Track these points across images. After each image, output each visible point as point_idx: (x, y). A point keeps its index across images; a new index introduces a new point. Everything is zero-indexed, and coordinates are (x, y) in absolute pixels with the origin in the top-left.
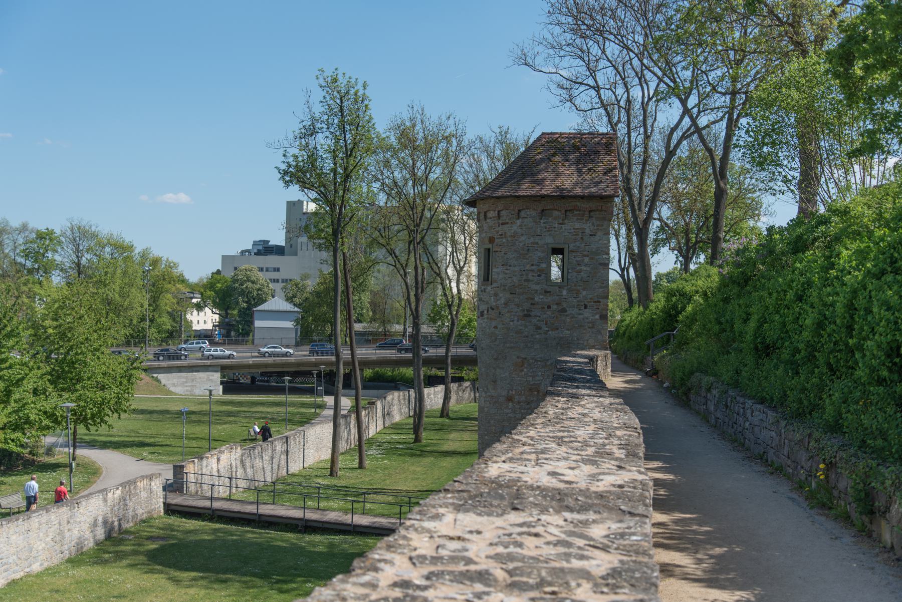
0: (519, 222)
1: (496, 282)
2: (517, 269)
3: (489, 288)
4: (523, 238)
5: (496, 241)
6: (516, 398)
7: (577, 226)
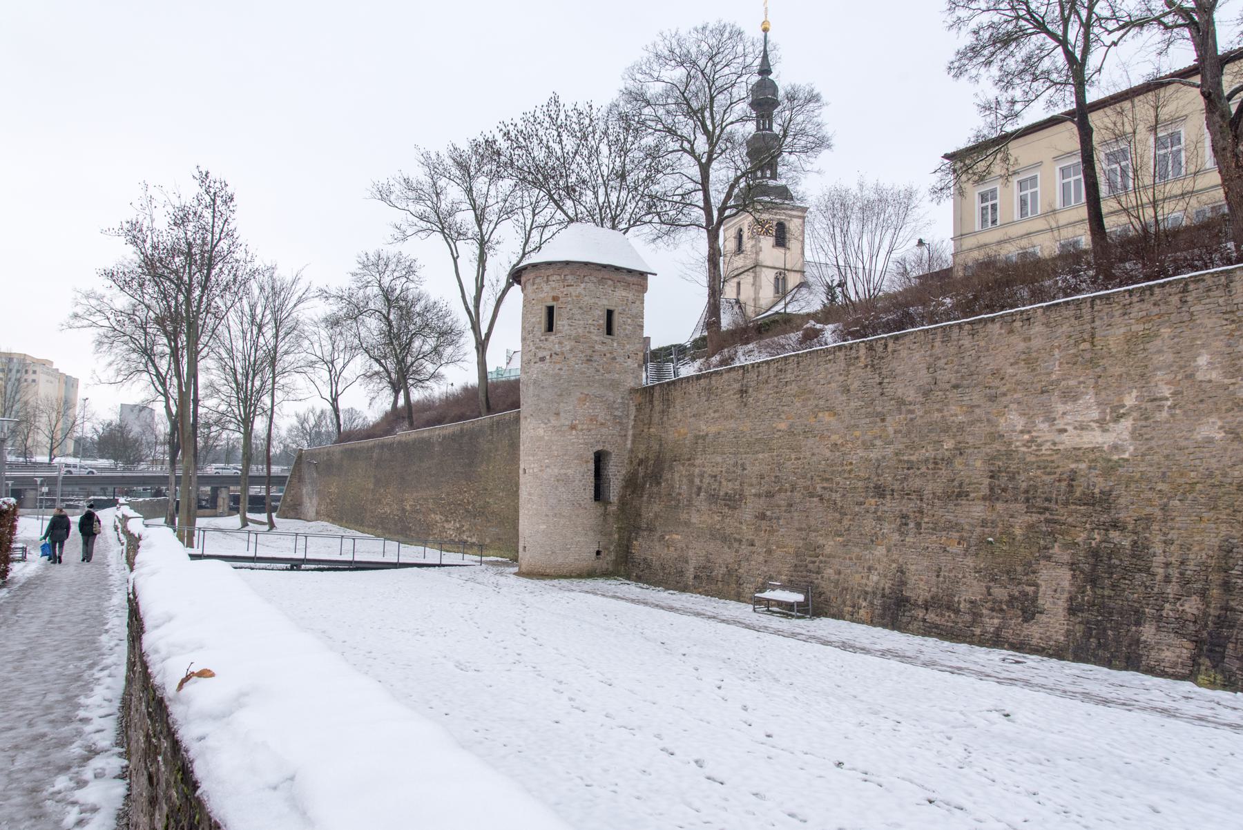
0: (583, 286)
2: (581, 322)
3: (553, 337)
4: (586, 298)
6: (580, 427)
7: (624, 294)
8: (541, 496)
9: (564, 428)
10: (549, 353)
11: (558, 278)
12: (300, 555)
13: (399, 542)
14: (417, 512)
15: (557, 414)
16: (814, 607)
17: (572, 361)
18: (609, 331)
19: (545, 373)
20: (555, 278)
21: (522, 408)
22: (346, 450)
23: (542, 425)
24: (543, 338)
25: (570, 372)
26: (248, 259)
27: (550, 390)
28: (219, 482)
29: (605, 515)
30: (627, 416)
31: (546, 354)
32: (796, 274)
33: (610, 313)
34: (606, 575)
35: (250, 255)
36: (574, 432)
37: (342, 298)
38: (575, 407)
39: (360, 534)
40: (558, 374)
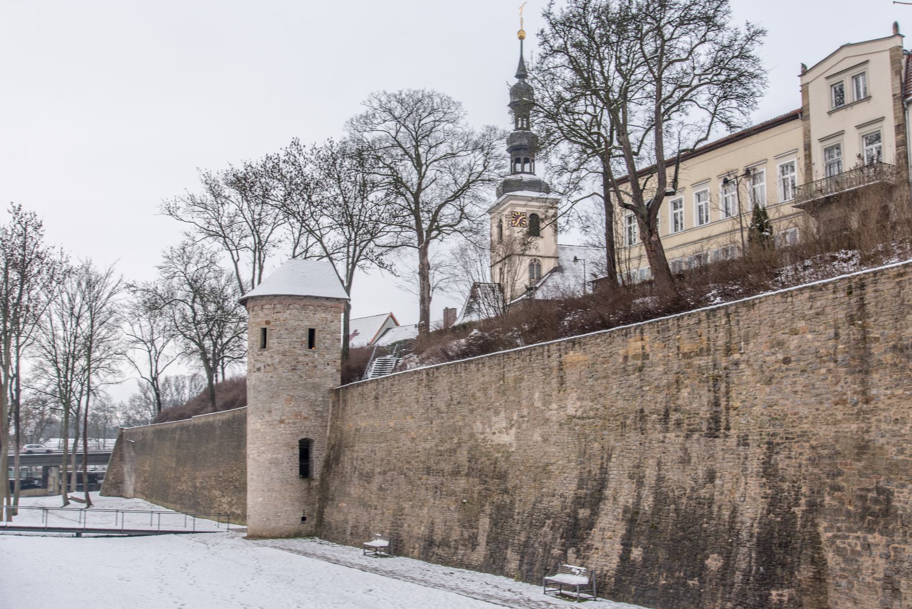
0: (288, 312)
2: (287, 340)
4: (291, 322)
6: (287, 421)
8: (258, 476)
9: (275, 422)
10: (263, 364)
11: (270, 306)
12: (81, 526)
13: (194, 516)
14: (203, 488)
15: (270, 412)
16: (396, 549)
17: (280, 370)
18: (311, 344)
19: (261, 380)
20: (267, 306)
21: (250, 407)
22: (157, 430)
23: (260, 421)
24: (259, 353)
25: (279, 379)
26: (64, 260)
27: (264, 393)
28: (49, 459)
29: (309, 489)
30: (328, 410)
32: (550, 259)
33: (312, 332)
34: (310, 535)
35: (65, 256)
36: (282, 425)
37: (148, 291)
38: (283, 406)
39: (164, 509)
40: (270, 381)
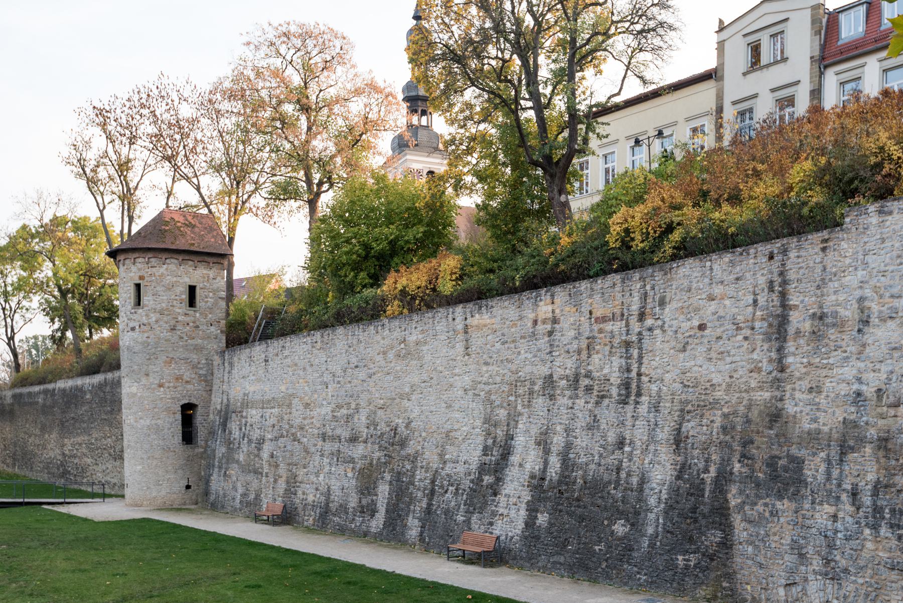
0: (165, 266)
1: (147, 306)
2: (165, 298)
5: (146, 279)
6: (167, 385)
10: (138, 324)
15: (147, 375)
20: (140, 260)
24: (133, 311)
25: (157, 340)
31: (136, 324)
36: (162, 389)
